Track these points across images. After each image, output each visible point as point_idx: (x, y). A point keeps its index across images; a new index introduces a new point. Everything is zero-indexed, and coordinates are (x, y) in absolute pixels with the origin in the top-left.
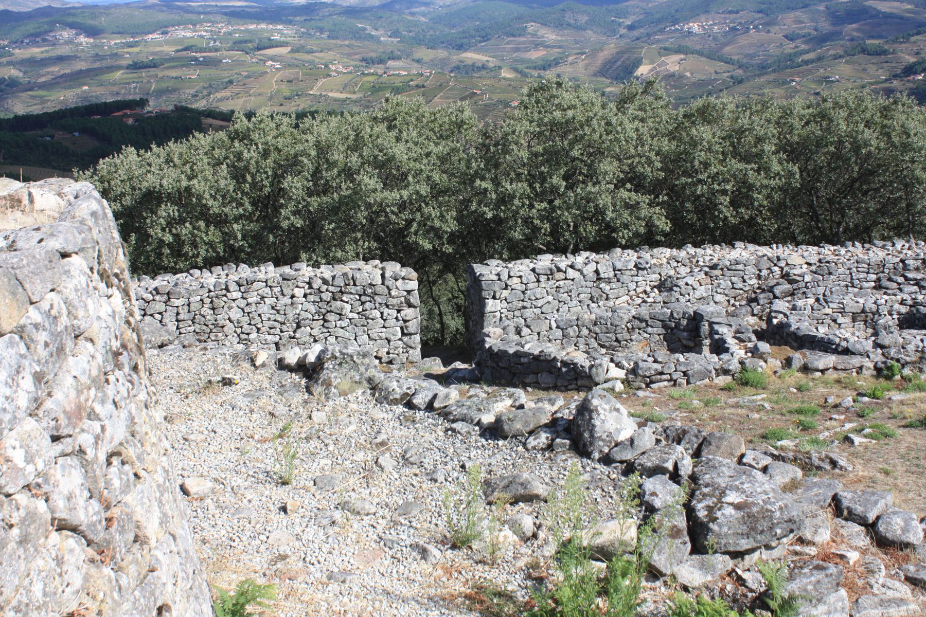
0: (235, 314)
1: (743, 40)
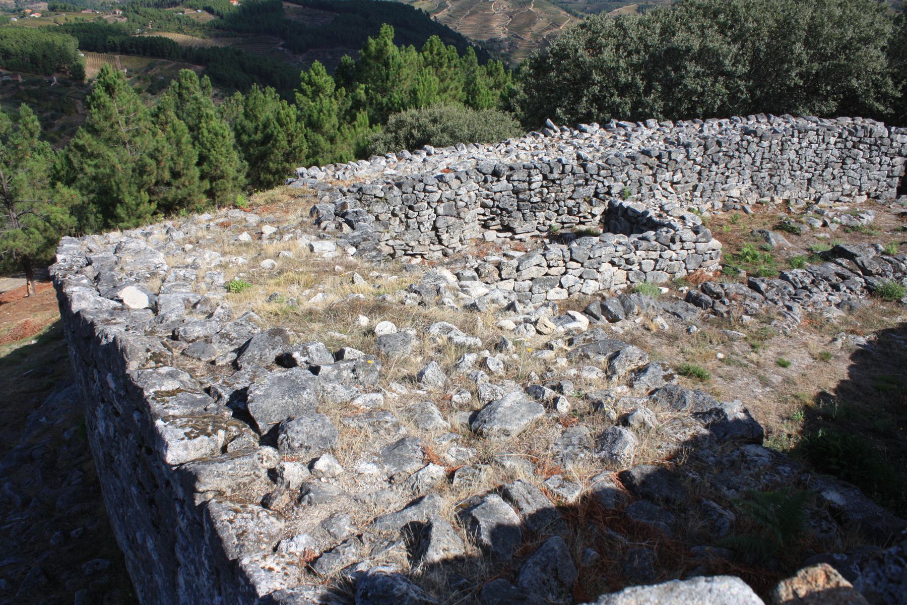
0: (792, 155)
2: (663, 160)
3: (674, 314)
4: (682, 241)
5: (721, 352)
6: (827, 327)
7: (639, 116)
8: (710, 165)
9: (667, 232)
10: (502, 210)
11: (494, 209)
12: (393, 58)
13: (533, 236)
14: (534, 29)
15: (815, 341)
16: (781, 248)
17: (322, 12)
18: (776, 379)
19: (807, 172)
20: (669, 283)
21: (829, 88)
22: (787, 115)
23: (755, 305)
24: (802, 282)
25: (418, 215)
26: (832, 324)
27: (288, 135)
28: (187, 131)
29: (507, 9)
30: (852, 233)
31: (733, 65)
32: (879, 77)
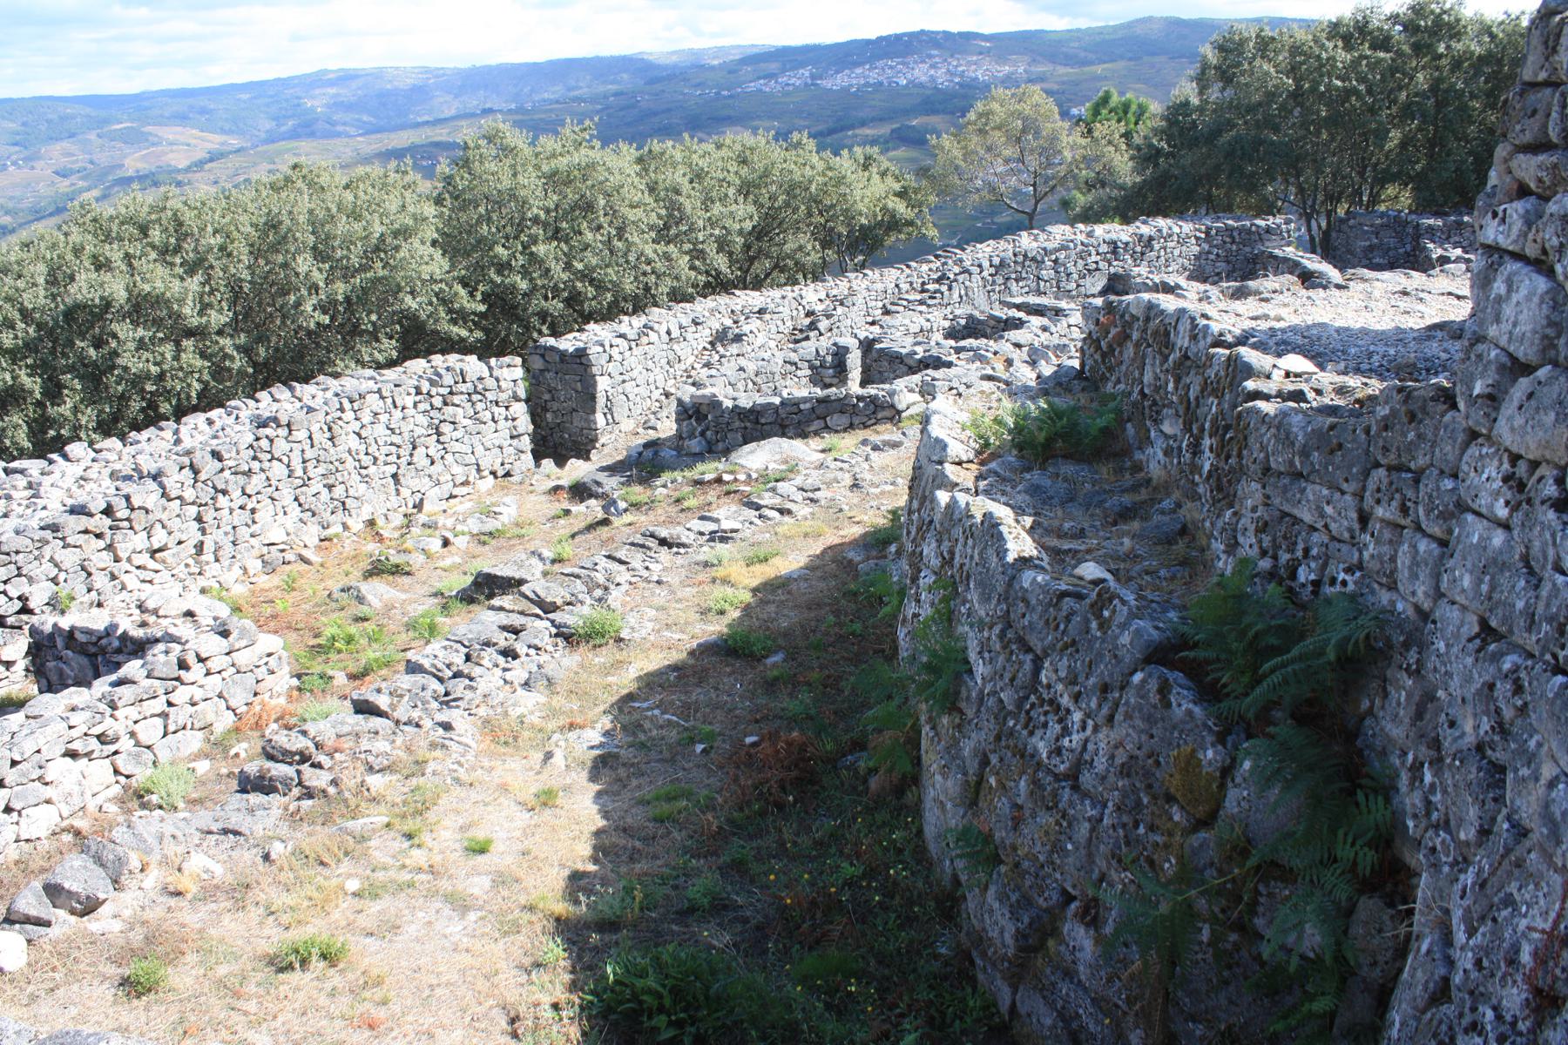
0: (354, 442)
2: (119, 515)
3: (225, 832)
4: (201, 660)
5: (349, 876)
6: (526, 734)
7: (47, 443)
9: (167, 652)
15: (519, 773)
16: (389, 607)
18: (479, 886)
19: (386, 464)
20: (207, 748)
21: (374, 317)
22: (321, 378)
23: (381, 745)
24: (448, 666)
26: (533, 727)
30: (493, 542)
31: (201, 313)
32: (443, 286)
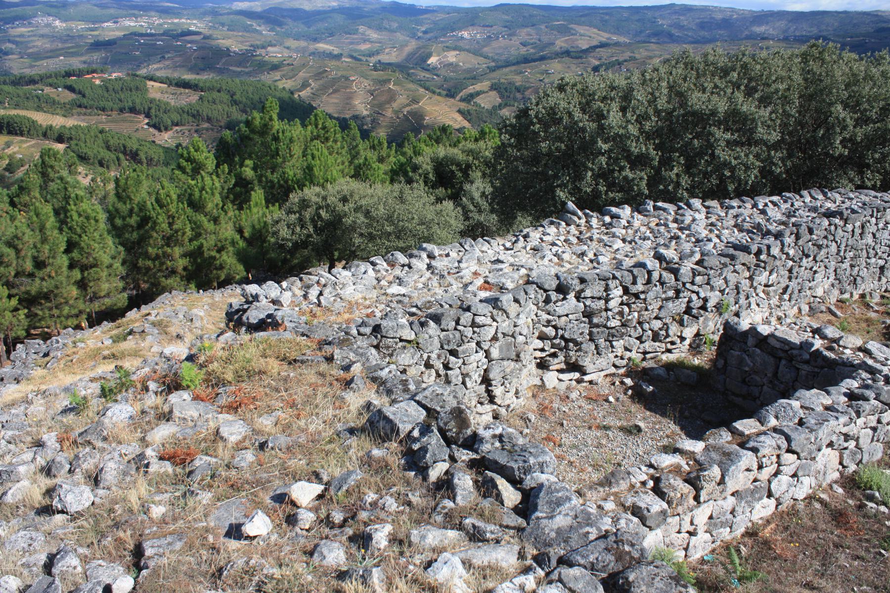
1: (495, 44)
8: (801, 259)
10: (567, 341)
11: (557, 341)
12: (283, 132)
13: (606, 376)
14: (395, 105)
17: (187, 91)
19: (880, 258)
25: (464, 363)
27: (169, 217)
28: (52, 214)
29: (368, 87)
